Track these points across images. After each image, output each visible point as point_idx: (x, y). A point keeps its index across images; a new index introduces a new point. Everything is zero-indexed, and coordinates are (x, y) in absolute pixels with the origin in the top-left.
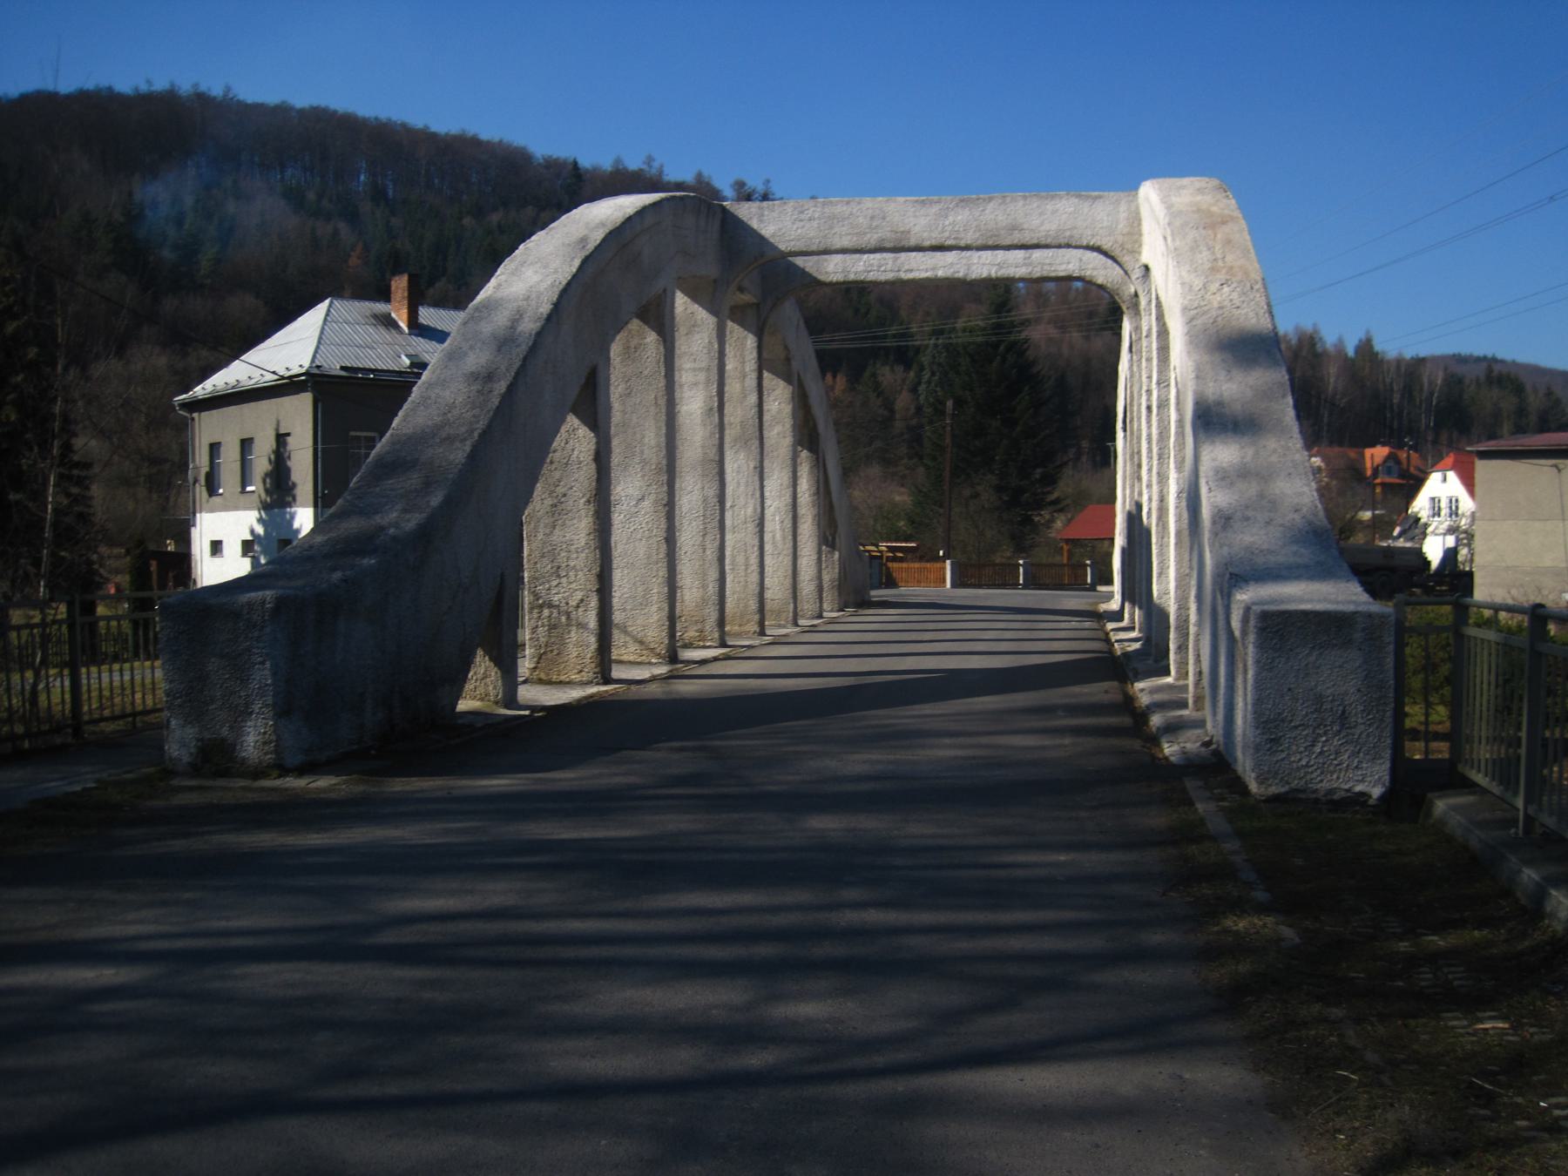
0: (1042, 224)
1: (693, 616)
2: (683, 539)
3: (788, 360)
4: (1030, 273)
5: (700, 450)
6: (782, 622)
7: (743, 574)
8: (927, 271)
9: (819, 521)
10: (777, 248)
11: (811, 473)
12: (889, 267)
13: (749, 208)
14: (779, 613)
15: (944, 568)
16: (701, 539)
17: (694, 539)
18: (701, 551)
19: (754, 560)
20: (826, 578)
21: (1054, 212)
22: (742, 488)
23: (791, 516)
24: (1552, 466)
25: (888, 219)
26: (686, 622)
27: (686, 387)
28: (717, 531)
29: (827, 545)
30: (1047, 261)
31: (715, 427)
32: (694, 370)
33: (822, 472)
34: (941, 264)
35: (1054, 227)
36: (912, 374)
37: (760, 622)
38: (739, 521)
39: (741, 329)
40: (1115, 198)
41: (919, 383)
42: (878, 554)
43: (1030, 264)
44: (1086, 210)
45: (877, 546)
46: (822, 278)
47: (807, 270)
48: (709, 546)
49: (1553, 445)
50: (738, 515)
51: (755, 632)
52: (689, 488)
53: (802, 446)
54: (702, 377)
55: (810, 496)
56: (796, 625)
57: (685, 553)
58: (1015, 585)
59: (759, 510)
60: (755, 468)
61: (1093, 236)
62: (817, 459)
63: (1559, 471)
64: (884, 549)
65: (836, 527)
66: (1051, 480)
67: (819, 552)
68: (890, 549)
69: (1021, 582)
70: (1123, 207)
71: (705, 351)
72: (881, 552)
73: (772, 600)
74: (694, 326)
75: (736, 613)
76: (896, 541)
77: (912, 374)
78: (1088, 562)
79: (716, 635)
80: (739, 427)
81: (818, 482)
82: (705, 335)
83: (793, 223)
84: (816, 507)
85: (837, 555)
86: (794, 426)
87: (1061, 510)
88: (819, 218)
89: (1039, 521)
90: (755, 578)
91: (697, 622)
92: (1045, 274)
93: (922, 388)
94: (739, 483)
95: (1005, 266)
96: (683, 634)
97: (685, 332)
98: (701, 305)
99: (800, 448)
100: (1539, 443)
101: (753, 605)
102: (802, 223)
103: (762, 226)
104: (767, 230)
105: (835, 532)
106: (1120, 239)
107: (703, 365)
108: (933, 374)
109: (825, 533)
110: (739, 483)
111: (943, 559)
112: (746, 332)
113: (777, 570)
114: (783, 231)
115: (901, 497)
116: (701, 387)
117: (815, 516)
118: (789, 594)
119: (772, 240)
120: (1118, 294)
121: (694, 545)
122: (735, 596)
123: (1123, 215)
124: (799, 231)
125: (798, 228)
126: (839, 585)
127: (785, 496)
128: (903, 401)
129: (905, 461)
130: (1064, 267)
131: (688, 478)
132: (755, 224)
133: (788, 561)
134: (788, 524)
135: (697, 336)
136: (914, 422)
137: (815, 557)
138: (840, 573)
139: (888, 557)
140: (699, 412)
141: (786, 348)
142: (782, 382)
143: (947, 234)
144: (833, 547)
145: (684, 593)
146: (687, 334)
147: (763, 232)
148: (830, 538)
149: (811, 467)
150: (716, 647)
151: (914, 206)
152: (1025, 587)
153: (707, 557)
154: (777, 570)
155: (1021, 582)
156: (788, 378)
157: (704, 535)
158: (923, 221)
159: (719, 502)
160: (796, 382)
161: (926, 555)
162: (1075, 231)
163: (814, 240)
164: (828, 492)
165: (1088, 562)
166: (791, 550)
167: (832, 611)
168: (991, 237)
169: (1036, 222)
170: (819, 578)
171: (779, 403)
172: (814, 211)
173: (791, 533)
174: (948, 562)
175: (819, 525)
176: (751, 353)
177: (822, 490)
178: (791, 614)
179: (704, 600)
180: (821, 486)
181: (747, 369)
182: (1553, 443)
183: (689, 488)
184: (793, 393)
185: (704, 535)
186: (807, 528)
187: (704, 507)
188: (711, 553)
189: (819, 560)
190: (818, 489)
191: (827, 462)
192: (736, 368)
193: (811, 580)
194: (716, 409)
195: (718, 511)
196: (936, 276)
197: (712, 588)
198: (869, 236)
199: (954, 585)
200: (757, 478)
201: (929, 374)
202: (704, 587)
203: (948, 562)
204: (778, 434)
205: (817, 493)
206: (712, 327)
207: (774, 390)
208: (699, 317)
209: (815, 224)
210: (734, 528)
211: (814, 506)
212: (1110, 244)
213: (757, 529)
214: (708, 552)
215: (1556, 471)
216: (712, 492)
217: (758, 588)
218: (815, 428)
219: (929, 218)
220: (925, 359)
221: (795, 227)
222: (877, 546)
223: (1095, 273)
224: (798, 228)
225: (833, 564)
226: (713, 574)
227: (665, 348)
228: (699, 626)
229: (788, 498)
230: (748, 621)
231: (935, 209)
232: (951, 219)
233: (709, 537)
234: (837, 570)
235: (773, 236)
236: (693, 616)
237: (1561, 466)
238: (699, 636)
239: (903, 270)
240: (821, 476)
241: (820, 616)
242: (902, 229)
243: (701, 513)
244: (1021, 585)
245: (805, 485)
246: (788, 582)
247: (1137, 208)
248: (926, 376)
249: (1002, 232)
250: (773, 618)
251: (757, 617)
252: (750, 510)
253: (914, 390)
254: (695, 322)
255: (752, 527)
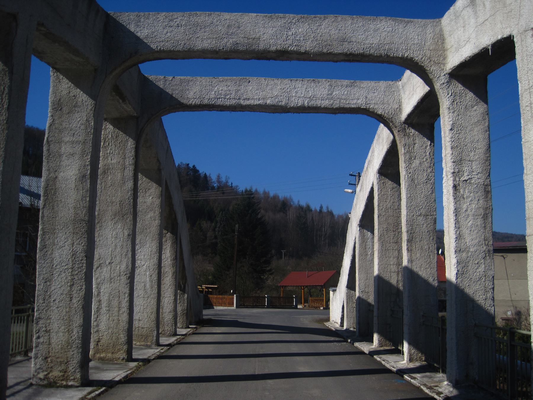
0: (366, 39)
1: (58, 358)
2: (53, 288)
3: (159, 170)
4: (332, 105)
5: (72, 211)
6: (149, 343)
7: (116, 314)
8: (259, 100)
9: (176, 276)
10: (149, 46)
11: (172, 246)
12: (233, 96)
13: (128, 16)
14: (146, 337)
15: (233, 298)
16: (69, 288)
17: (63, 288)
18: (68, 299)
19: (125, 304)
20: (179, 309)
21: (375, 31)
22: (118, 249)
23: (157, 272)
24: (501, 256)
25: (242, 28)
26: (51, 362)
27: (64, 157)
28: (83, 282)
29: (180, 290)
30: (343, 97)
31: (87, 191)
32: (73, 142)
33: (179, 246)
34: (270, 95)
35: (376, 41)
36: (213, 224)
37: (128, 351)
38: (115, 274)
39: (124, 135)
40: (422, 23)
41: (216, 227)
42: (202, 290)
43: (332, 99)
44: (401, 30)
45: (201, 286)
46: (185, 101)
47: (174, 96)
48: (75, 295)
49: (502, 247)
50: (115, 270)
51: (123, 359)
52: (61, 244)
53: (167, 230)
54: (78, 149)
55: (171, 260)
56: (158, 344)
57: (54, 301)
58: (263, 306)
59: (130, 267)
60: (129, 235)
61: (407, 50)
62: (176, 238)
63: (504, 258)
64: (204, 287)
65: (186, 279)
66: (268, 262)
67: (176, 295)
68: (207, 288)
69: (266, 305)
70: (429, 30)
71: (82, 127)
72: (203, 289)
73: (142, 328)
74: (75, 106)
75: (110, 344)
76: (209, 285)
77: (213, 224)
78: (294, 296)
79: (78, 376)
80: (118, 205)
81: (176, 252)
82: (84, 115)
83: (164, 28)
84: (175, 267)
85: (186, 296)
86: (161, 213)
87: (271, 274)
88: (186, 25)
89: (263, 278)
90: (125, 317)
91: (61, 363)
92: (342, 105)
93: (217, 229)
94: (116, 246)
95: (314, 99)
96: (49, 373)
97: (67, 112)
98: (82, 89)
99: (165, 232)
100: (496, 246)
101: (123, 338)
102: (171, 29)
103: (138, 29)
104: (142, 33)
105: (185, 283)
106: (428, 53)
107: (81, 138)
108: (221, 224)
109: (179, 283)
110: (116, 246)
111: (233, 295)
112: (128, 137)
113: (146, 308)
114: (155, 34)
115: (210, 268)
116: (77, 157)
117: (174, 273)
118: (153, 325)
119: (145, 41)
120: (392, 122)
121: (62, 294)
122: (110, 331)
123: (429, 36)
124: (169, 34)
125: (167, 33)
126: (187, 313)
127: (153, 258)
128: (210, 234)
129: (210, 255)
130: (355, 101)
131: (60, 235)
132: (132, 28)
133: (154, 302)
134: (155, 277)
135: (77, 115)
136: (214, 241)
137: (173, 298)
138: (187, 306)
139: (205, 291)
140: (74, 178)
141: (158, 160)
142: (155, 184)
143: (290, 42)
144: (184, 291)
145: (51, 336)
146: (68, 113)
147: (139, 34)
148: (182, 286)
149: (172, 243)
150: (77, 387)
151: (264, 20)
152: (268, 307)
153: (74, 304)
154: (146, 308)
155: (266, 305)
156: (159, 182)
157: (72, 286)
158: (270, 31)
159: (86, 256)
160: (164, 186)
161: (222, 291)
162: (393, 45)
163: (180, 42)
164: (182, 259)
165: (294, 296)
166: (156, 295)
167: (182, 328)
168: (326, 46)
169: (361, 37)
170: (175, 310)
171: (152, 198)
172: (181, 20)
173: (156, 283)
174: (235, 295)
175: (176, 278)
176: (131, 152)
177: (178, 257)
178: (155, 338)
179: (69, 344)
180: (178, 254)
181: (127, 163)
182: (502, 246)
183: (61, 244)
184: (161, 192)
185: (72, 286)
186: (168, 281)
187: (72, 261)
188: (77, 302)
189: (175, 300)
190: (176, 256)
191: (182, 241)
192: (119, 162)
193: (170, 312)
194: (88, 176)
195: (84, 265)
196: (266, 103)
197: (76, 333)
198: (225, 40)
199: (237, 307)
200: (129, 243)
201: (219, 224)
202: (70, 332)
203: (235, 295)
204: (151, 218)
205: (175, 259)
206: (90, 108)
207: (149, 189)
208: (80, 100)
209: (182, 30)
210: (111, 279)
211: (173, 267)
212: (420, 57)
213: (128, 281)
214: (74, 301)
215: (503, 258)
216: (80, 248)
217: (127, 325)
218: (175, 219)
219: (275, 29)
220: (218, 219)
221: (165, 31)
222: (201, 286)
223: (376, 107)
224: (167, 33)
225: (184, 300)
226: (78, 320)
227: (11, 79)
228: (63, 367)
229: (155, 260)
230: (119, 350)
231: (281, 22)
232: (293, 31)
233: (76, 288)
234: (186, 305)
235: (147, 37)
236: (58, 358)
237: (505, 256)
238: (63, 376)
239: (242, 98)
240: (178, 249)
241: (175, 334)
242: (254, 36)
243: (70, 265)
244: (266, 306)
245: (168, 254)
246: (153, 317)
247: (441, 30)
248: (218, 225)
249: (334, 43)
250: (142, 340)
251: (125, 347)
252: (123, 266)
253: (214, 230)
254: (77, 103)
255: (124, 279)
